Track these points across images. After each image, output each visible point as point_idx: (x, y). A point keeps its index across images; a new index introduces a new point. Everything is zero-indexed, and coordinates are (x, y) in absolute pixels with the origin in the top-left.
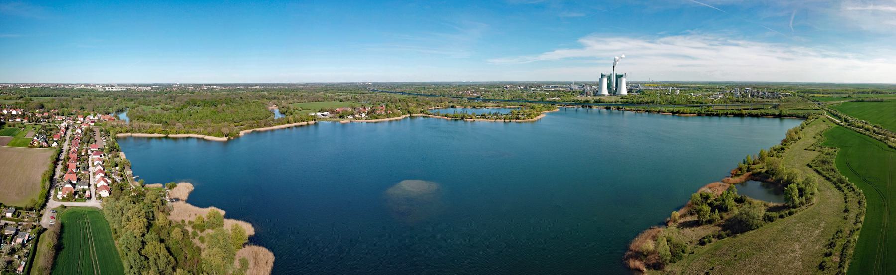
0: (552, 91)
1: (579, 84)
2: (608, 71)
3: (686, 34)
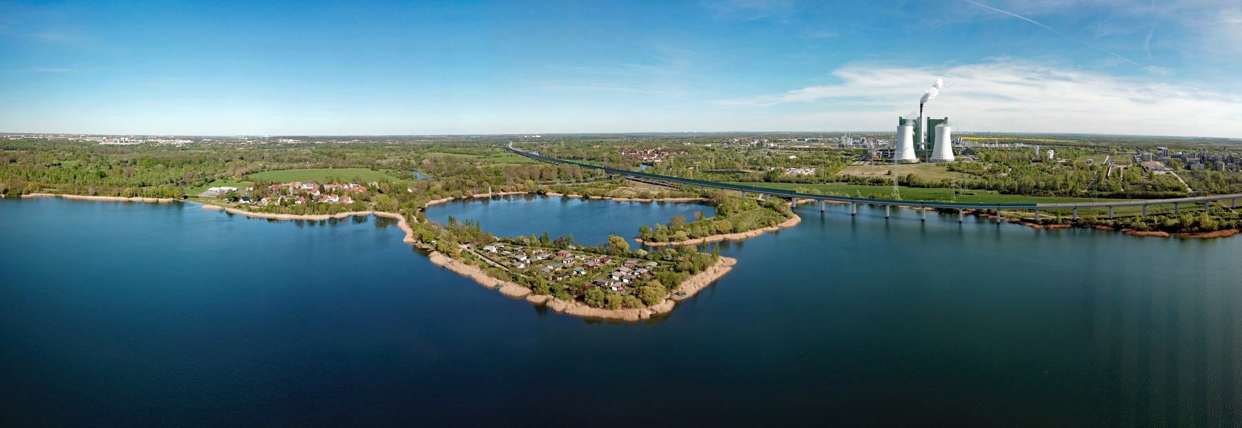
0: (805, 149)
1: (854, 136)
2: (910, 112)
3: (990, 62)
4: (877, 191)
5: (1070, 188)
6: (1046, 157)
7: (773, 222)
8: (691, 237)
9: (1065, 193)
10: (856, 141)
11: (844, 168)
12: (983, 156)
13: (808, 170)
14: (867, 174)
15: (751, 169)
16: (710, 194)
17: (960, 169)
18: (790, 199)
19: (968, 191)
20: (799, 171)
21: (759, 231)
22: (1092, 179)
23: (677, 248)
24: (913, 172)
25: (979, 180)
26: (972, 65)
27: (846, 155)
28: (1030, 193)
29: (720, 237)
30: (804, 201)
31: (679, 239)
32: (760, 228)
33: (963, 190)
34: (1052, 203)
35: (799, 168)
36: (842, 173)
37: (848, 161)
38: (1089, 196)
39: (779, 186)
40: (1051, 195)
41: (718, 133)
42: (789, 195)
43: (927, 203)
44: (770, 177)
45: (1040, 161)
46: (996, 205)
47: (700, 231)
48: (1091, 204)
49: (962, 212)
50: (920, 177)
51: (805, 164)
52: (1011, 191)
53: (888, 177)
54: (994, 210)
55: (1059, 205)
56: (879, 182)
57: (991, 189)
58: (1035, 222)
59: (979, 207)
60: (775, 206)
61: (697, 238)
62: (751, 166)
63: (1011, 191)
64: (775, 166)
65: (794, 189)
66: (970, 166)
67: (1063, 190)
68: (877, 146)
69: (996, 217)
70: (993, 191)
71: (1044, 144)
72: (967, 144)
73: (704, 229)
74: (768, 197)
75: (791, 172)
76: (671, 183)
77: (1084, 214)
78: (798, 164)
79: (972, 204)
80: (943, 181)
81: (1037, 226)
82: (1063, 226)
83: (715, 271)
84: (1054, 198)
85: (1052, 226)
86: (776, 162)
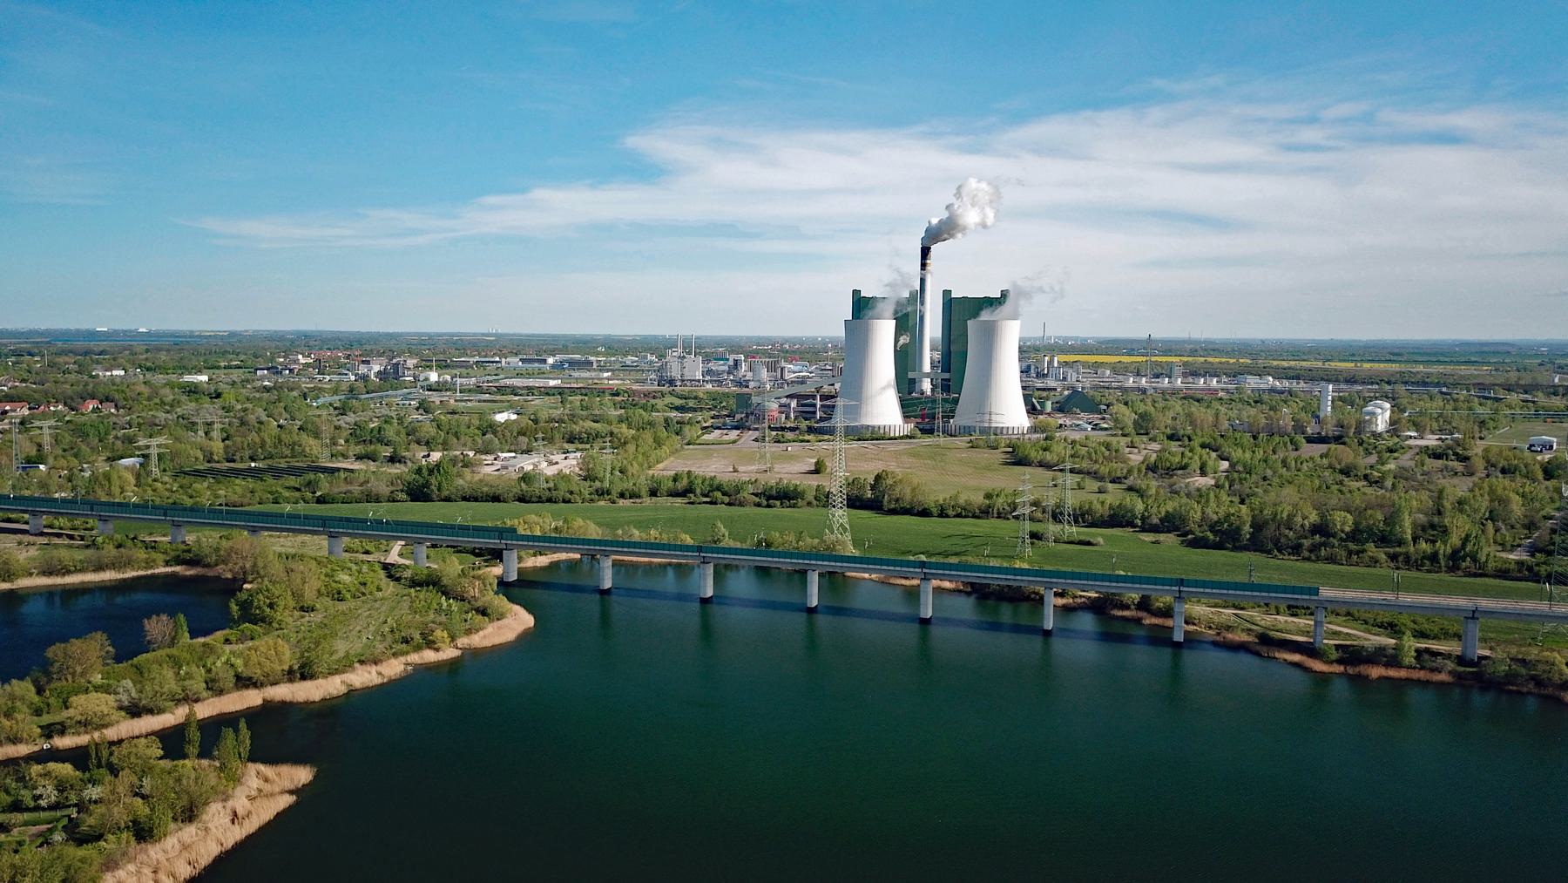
0: (547, 392)
1: (706, 350)
4: (781, 525)
5: (1455, 540)
6: (1360, 427)
7: (439, 634)
8: (135, 711)
9: (1434, 557)
10: (713, 366)
11: (674, 452)
12: (1128, 416)
13: (558, 457)
14: (748, 471)
15: (359, 458)
16: (207, 551)
17: (1048, 457)
18: (496, 555)
19: (1073, 531)
20: (527, 464)
21: (394, 668)
22: (1549, 510)
23: (78, 757)
24: (892, 467)
25: (1114, 496)
26: (1089, 113)
27: (677, 409)
28: (1296, 549)
29: (253, 698)
30: (543, 561)
31: (85, 724)
32: (395, 655)
33: (1059, 527)
34: (1380, 590)
35: (528, 451)
36: (668, 467)
37: (686, 428)
38: (1536, 578)
39: (461, 514)
40: (1375, 562)
41: (232, 334)
42: (493, 543)
43: (937, 566)
44: (427, 485)
45: (1338, 439)
46: (1171, 582)
47: (172, 685)
48: (1543, 606)
49: (1052, 601)
50: (916, 481)
51: (549, 440)
52: (1225, 537)
53: (813, 481)
54: (1164, 599)
55: (1407, 598)
56: (785, 496)
57: (1154, 529)
58: (1310, 650)
59: (1112, 588)
60: (445, 581)
61: (161, 711)
62: (360, 449)
63: (1225, 537)
64: (445, 446)
65: (509, 523)
66: (1083, 451)
67: (1424, 546)
68: (780, 381)
69: (1169, 623)
70: (1162, 537)
71: (1351, 380)
72: (1072, 377)
73: (189, 676)
74: (423, 550)
75: (498, 464)
76: (45, 519)
77: (1512, 642)
78: (523, 440)
79: (1088, 577)
80: (988, 496)
81: (1318, 666)
82: (1421, 675)
83: (235, 814)
84: (1384, 571)
85: (1376, 672)
86: (448, 434)
